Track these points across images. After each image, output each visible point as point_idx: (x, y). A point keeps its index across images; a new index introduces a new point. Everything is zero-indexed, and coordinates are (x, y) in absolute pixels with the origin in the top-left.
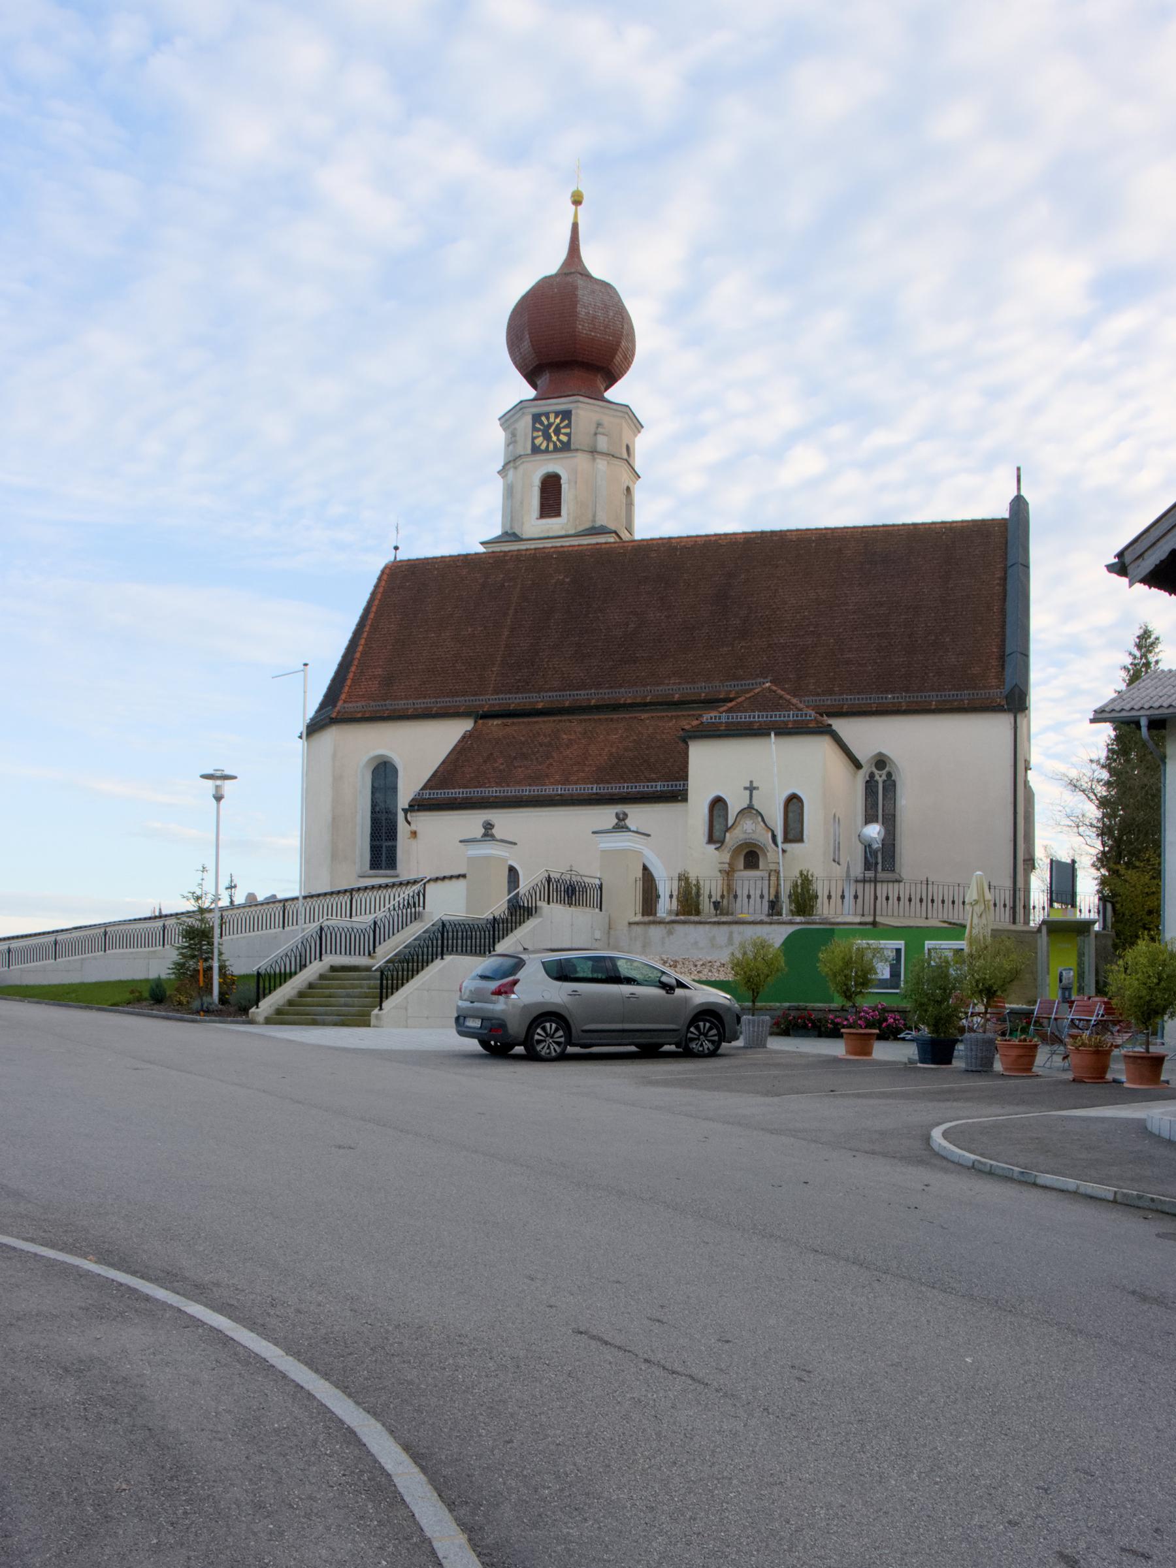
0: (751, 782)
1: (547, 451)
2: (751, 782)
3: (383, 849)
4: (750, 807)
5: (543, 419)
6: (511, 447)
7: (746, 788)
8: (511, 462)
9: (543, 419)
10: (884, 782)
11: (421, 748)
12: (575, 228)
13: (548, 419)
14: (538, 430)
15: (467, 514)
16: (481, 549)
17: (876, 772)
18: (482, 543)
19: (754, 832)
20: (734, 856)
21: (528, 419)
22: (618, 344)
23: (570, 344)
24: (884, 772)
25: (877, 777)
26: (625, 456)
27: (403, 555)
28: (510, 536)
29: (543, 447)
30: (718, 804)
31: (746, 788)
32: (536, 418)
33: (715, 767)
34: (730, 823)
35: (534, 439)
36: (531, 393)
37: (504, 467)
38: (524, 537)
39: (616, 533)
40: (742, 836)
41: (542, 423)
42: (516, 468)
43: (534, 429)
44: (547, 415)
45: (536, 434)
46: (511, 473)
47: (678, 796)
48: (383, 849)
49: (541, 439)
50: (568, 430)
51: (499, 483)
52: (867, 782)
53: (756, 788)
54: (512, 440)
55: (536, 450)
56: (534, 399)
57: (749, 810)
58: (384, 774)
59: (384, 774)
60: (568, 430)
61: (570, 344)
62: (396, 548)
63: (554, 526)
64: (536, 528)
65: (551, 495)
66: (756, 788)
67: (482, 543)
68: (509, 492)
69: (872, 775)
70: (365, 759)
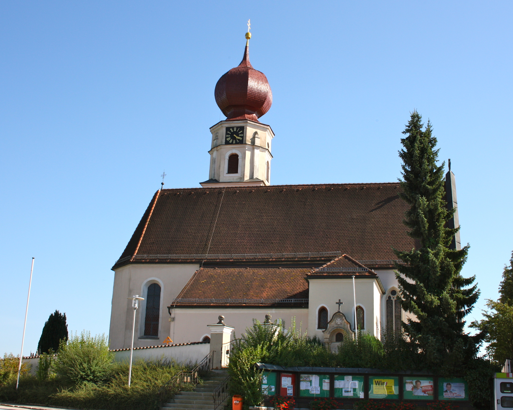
0: (340, 300)
1: (232, 144)
2: (340, 300)
3: (151, 328)
4: (339, 312)
5: (231, 129)
6: (215, 141)
7: (337, 303)
8: (215, 147)
9: (231, 129)
10: (395, 301)
11: (174, 278)
12: (246, 47)
13: (233, 130)
14: (228, 134)
15: (192, 172)
16: (200, 186)
17: (392, 296)
18: (200, 183)
19: (341, 324)
20: (331, 336)
21: (224, 130)
22: (265, 99)
23: (238, 99)
24: (395, 296)
25: (392, 299)
26: (267, 148)
27: (165, 187)
28: (212, 181)
29: (231, 142)
30: (323, 311)
31: (337, 303)
32: (228, 129)
33: (323, 293)
34: (329, 320)
35: (226, 138)
36: (225, 118)
37: (211, 149)
38: (220, 181)
39: (263, 181)
40: (335, 326)
41: (230, 131)
42: (217, 150)
43: (227, 134)
44: (233, 128)
45: (227, 136)
46: (215, 153)
47: (305, 305)
48: (151, 328)
49: (230, 138)
50: (242, 135)
51: (208, 157)
52: (387, 301)
53: (342, 303)
54: (215, 138)
55: (227, 143)
56: (226, 121)
57: (338, 314)
58: (154, 291)
59: (154, 291)
60: (242, 135)
61: (238, 99)
62: (162, 184)
63: (233, 177)
64: (226, 178)
65: (234, 164)
66: (342, 303)
67: (200, 183)
68: (213, 161)
69: (390, 297)
70: (145, 282)
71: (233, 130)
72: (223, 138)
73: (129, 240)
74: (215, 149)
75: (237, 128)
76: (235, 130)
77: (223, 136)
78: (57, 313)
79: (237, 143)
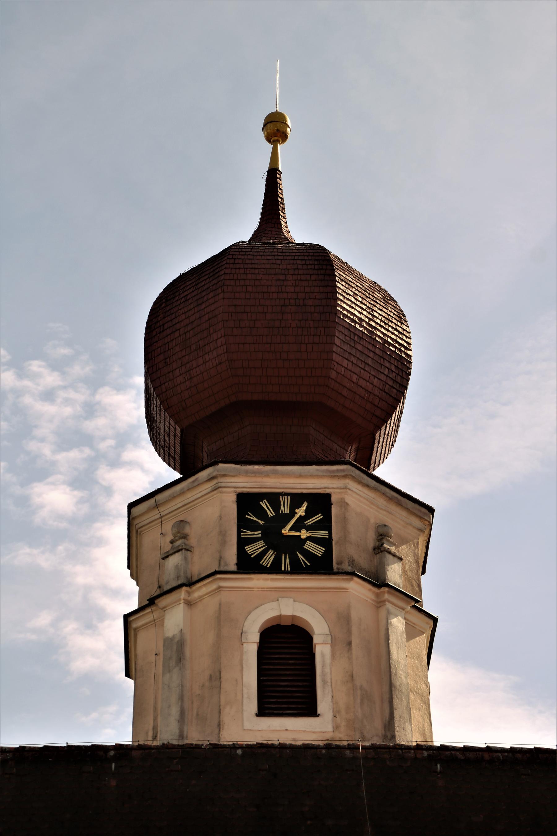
1: (275, 569)
5: (264, 504)
9: (264, 504)
14: (254, 526)
29: (269, 559)
35: (242, 543)
41: (262, 514)
42: (189, 604)
43: (243, 523)
44: (274, 498)
45: (247, 533)
55: (248, 565)
62: (275, 129)
71: (276, 505)
72: (224, 543)
73: (408, 493)
74: (183, 593)
75: (297, 499)
76: (285, 509)
77: (223, 534)
78: (329, 496)
79: (297, 569)
